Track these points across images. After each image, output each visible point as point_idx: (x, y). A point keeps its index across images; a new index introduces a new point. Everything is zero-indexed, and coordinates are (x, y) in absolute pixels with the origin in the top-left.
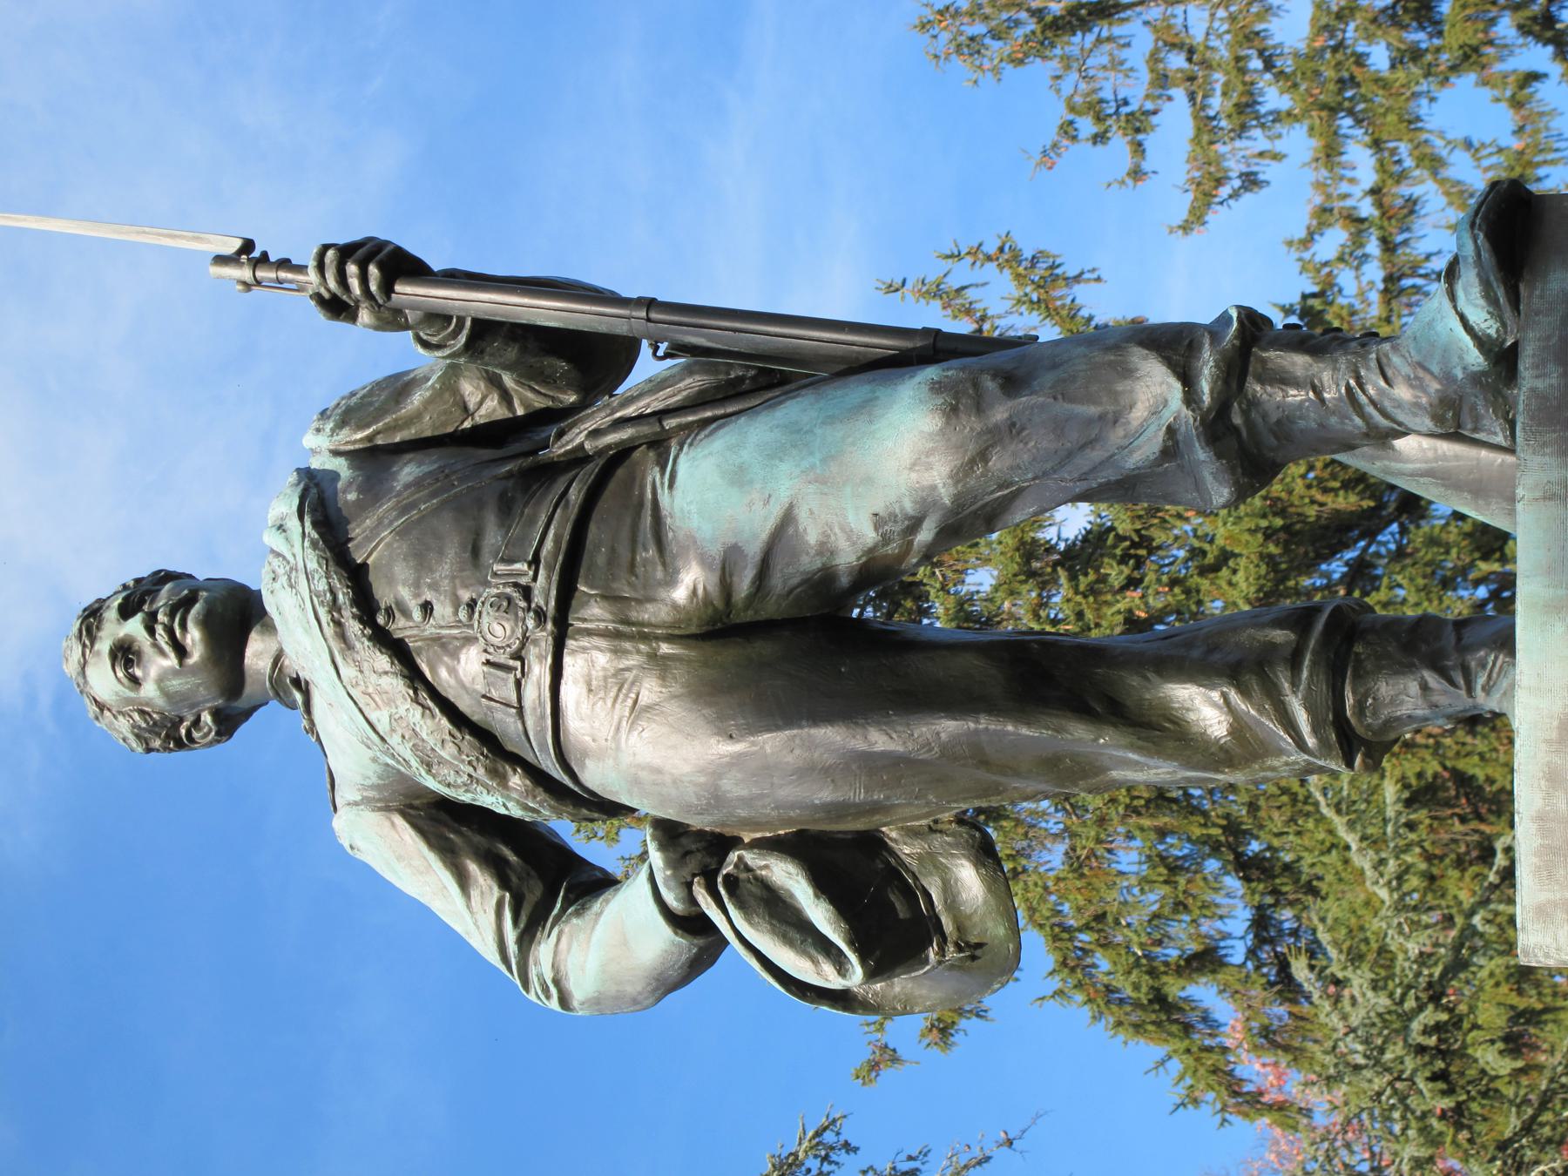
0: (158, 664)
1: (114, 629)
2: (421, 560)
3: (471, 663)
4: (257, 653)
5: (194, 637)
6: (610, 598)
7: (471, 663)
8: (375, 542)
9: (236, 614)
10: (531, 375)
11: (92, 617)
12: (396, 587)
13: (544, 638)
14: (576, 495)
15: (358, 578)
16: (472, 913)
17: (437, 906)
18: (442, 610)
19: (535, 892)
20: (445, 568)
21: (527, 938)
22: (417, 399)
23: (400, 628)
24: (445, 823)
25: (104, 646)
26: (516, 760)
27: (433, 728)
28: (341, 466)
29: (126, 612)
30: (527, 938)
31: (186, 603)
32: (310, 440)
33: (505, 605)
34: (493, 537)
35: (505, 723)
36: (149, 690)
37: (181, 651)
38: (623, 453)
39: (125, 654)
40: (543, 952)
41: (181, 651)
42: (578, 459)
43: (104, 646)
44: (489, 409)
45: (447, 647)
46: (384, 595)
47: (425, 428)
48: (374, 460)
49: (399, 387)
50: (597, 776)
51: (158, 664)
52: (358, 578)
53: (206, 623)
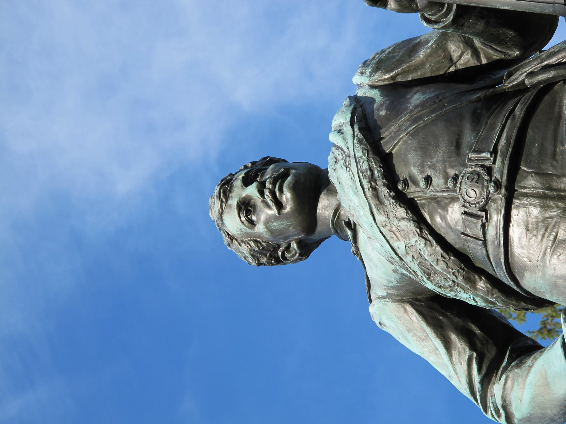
0: (266, 213)
1: (240, 192)
2: (425, 151)
3: (455, 213)
4: (325, 207)
5: (287, 197)
6: (540, 174)
7: (455, 213)
8: (398, 140)
9: (313, 183)
10: (491, 39)
11: (226, 186)
12: (409, 167)
13: (500, 198)
14: (519, 112)
15: (386, 162)
16: (452, 365)
17: (432, 360)
18: (438, 181)
19: (491, 353)
20: (439, 156)
21: (486, 381)
22: (422, 54)
23: (412, 192)
24: (438, 310)
25: (234, 202)
26: (482, 272)
27: (431, 252)
28: (375, 94)
29: (247, 182)
30: (486, 381)
31: (283, 177)
32: (357, 79)
33: (476, 178)
34: (468, 137)
35: (475, 250)
36: (260, 228)
37: (279, 205)
38: (549, 86)
39: (246, 207)
40: (497, 389)
41: (279, 205)
42: (521, 89)
43: (234, 202)
44: (466, 60)
45: (441, 204)
46: (402, 172)
47: (427, 72)
48: (395, 91)
49: (411, 47)
50: (531, 282)
51: (266, 213)
52: (386, 162)
53: (294, 189)
